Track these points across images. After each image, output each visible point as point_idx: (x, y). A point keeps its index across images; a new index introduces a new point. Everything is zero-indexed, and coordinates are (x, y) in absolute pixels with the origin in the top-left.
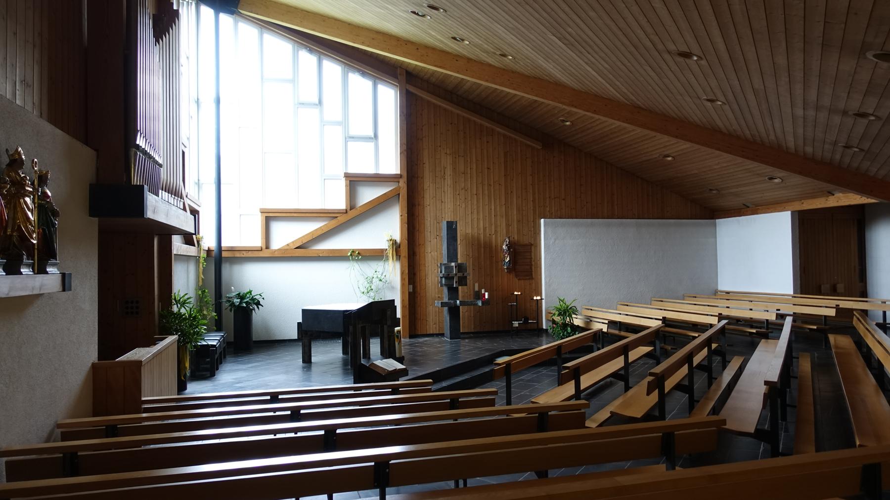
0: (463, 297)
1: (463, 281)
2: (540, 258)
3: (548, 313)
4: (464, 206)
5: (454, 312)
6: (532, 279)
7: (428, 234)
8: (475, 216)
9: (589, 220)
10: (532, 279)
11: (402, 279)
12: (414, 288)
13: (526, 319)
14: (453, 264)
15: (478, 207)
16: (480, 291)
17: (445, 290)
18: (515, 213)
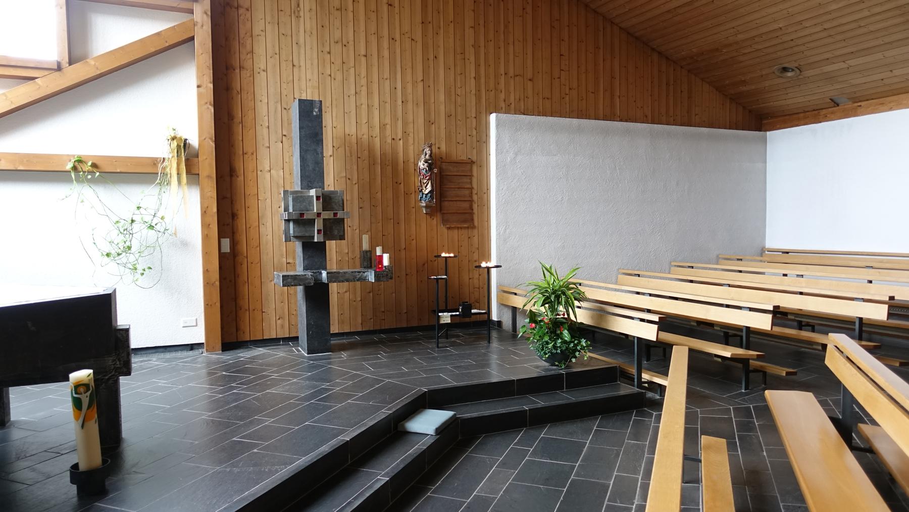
0: (339, 262)
1: (334, 228)
2: (488, 189)
3: (504, 292)
4: (339, 76)
5: (317, 296)
6: (474, 227)
7: (262, 132)
8: (364, 100)
9: (575, 122)
10: (474, 227)
11: (205, 225)
12: (234, 244)
13: (467, 308)
14: (313, 192)
15: (369, 83)
16: (372, 251)
17: (298, 247)
18: (442, 97)
